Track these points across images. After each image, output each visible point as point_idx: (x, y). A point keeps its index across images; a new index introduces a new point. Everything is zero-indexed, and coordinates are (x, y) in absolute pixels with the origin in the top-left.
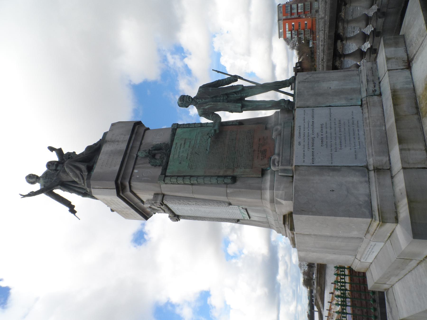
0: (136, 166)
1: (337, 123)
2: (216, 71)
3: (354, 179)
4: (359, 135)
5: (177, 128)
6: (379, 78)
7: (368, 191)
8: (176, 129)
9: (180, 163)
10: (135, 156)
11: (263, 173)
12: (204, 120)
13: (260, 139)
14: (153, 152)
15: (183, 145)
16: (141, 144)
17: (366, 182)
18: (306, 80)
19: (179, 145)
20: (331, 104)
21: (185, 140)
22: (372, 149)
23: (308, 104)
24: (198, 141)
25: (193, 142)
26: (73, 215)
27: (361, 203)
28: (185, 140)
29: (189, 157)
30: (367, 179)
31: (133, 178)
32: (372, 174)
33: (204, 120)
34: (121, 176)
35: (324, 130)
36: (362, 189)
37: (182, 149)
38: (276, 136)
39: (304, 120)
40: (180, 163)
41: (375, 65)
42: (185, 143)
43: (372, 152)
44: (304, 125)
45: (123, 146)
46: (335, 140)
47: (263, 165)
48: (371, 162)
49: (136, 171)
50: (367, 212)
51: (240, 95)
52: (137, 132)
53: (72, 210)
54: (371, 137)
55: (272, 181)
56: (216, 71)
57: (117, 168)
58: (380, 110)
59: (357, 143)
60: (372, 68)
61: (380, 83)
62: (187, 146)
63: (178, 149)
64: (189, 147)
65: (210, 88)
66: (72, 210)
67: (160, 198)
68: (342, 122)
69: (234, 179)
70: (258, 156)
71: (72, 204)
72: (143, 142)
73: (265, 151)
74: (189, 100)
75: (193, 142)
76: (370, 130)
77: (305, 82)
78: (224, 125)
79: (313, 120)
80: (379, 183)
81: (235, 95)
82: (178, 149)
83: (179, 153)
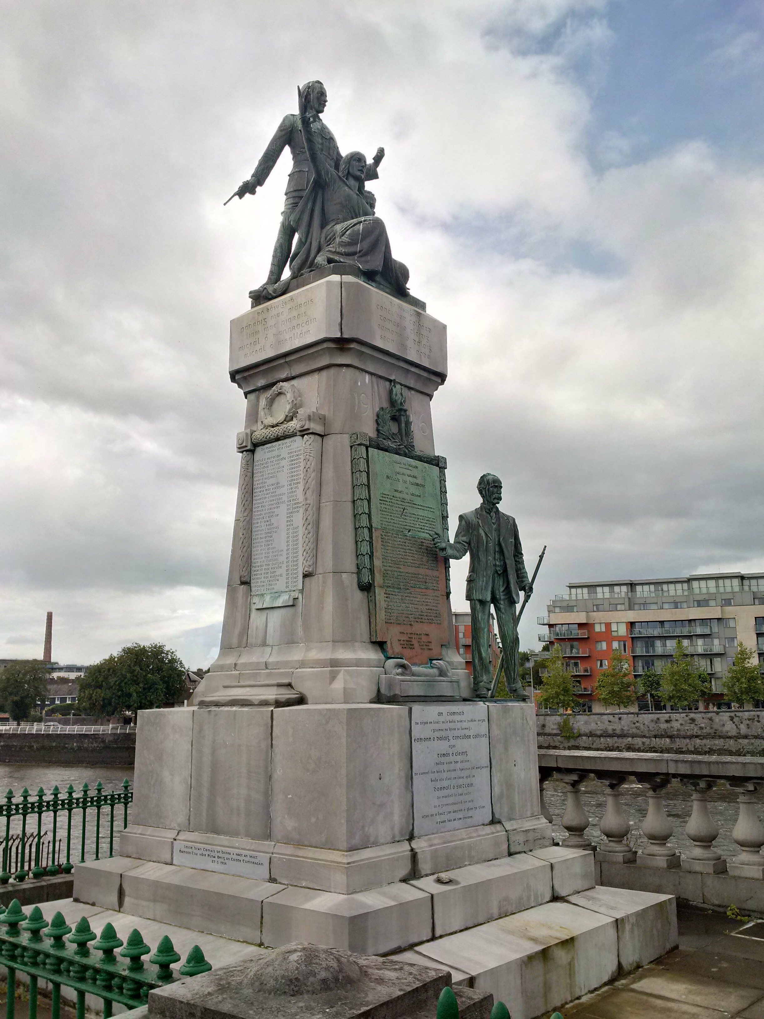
0: (374, 379)
1: (468, 781)
2: (543, 553)
3: (397, 817)
4: (455, 820)
5: (440, 468)
6: (531, 851)
7: (382, 841)
8: (437, 465)
9: (388, 477)
10: (392, 378)
11: (381, 645)
12: (453, 525)
13: (427, 635)
14: (403, 419)
15: (415, 481)
16: (410, 388)
17: (394, 837)
18: (525, 722)
19: (414, 472)
20: (493, 769)
21: (423, 486)
22: (439, 844)
23: (494, 727)
24: (421, 513)
25: (418, 501)
26: (236, 189)
27: (366, 829)
28: (423, 486)
29: (397, 494)
30: (397, 839)
31: (357, 372)
32: (405, 847)
33: (453, 525)
34: (364, 349)
35: (459, 758)
36: (382, 830)
37: (408, 479)
38: (438, 668)
39: (472, 721)
40: (388, 477)
41: (548, 844)
42: (417, 485)
43: (435, 845)
44: (465, 721)
45: (412, 356)
46: (447, 779)
47: (391, 643)
48: (419, 845)
49: (367, 377)
50: (356, 841)
51: (502, 597)
52: (430, 380)
53: (247, 189)
54: (454, 841)
55: (368, 663)
56: (543, 553)
57: (379, 344)
58: (491, 856)
59: (444, 818)
60: (544, 838)
61: (525, 852)
62: (413, 489)
63: (409, 472)
64: (412, 495)
65: (513, 540)
66: (247, 189)
67: (318, 428)
68: (470, 789)
69: (366, 588)
70: (403, 633)
71: (258, 189)
72: (413, 392)
73: (411, 647)
74: (494, 499)
75: (418, 501)
76: (463, 839)
77: (523, 720)
78: (445, 564)
79: (472, 737)
80: (397, 859)
81: (502, 589)
82: (409, 472)
83: (403, 474)
